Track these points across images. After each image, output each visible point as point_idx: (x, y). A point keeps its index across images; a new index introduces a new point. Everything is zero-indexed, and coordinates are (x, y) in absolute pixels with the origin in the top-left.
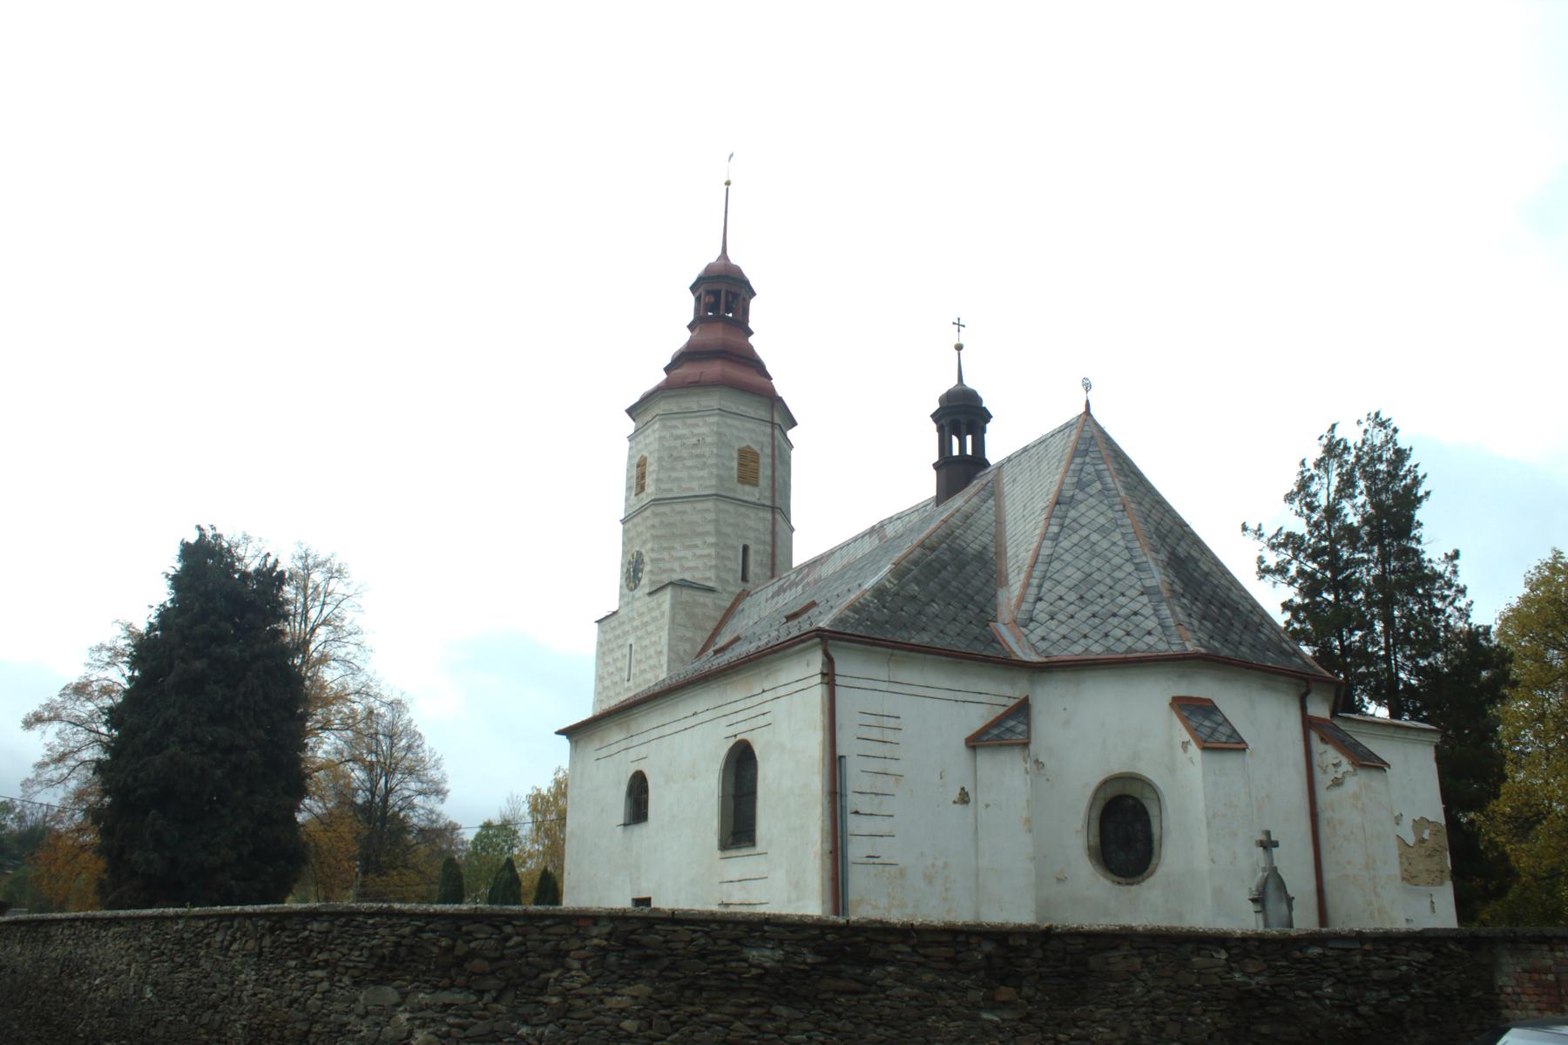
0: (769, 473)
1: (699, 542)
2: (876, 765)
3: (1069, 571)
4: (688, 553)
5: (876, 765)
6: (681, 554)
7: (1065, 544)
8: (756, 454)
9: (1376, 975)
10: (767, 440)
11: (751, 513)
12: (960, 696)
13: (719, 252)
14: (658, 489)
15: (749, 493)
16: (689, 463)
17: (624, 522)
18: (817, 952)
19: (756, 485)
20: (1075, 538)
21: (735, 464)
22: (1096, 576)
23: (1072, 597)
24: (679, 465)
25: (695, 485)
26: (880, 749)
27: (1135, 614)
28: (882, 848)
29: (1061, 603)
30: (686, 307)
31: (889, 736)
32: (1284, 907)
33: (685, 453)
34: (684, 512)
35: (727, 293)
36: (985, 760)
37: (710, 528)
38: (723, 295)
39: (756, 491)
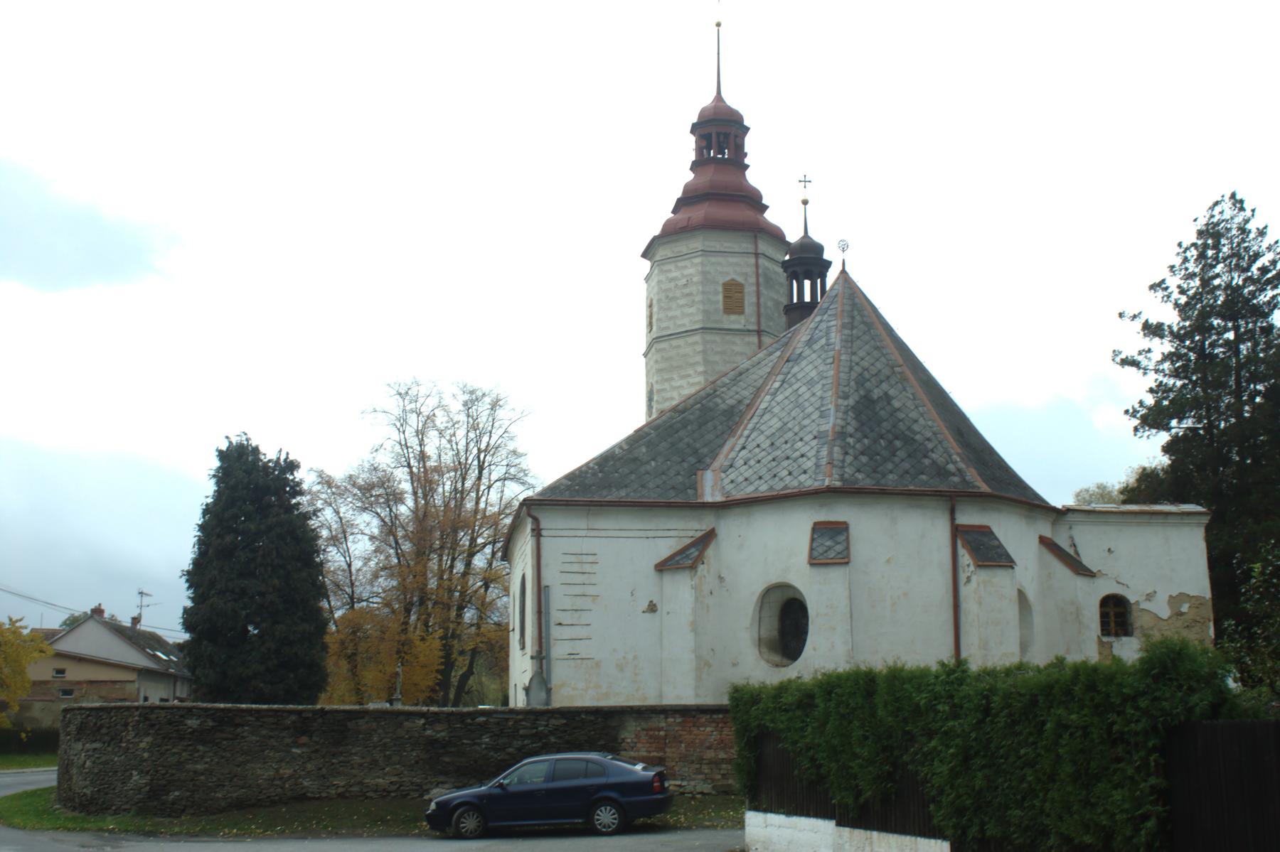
0: (754, 300)
1: (691, 372)
2: (578, 590)
3: (775, 420)
4: (683, 382)
5: (578, 590)
6: (678, 384)
7: (780, 398)
8: (741, 285)
9: (521, 732)
10: (751, 270)
11: (737, 339)
12: (650, 534)
13: (714, 93)
14: (659, 328)
15: (736, 322)
16: (682, 302)
17: (645, 355)
18: (214, 720)
19: (742, 312)
20: (790, 390)
21: (720, 297)
22: (790, 425)
23: (766, 445)
24: (674, 305)
25: (686, 321)
26: (579, 579)
27: (802, 456)
28: (580, 647)
29: (757, 450)
30: (688, 148)
31: (587, 568)
32: (543, 695)
33: (678, 293)
34: (679, 347)
35: (718, 135)
36: (667, 578)
37: (699, 358)
38: (720, 134)
39: (742, 319)
